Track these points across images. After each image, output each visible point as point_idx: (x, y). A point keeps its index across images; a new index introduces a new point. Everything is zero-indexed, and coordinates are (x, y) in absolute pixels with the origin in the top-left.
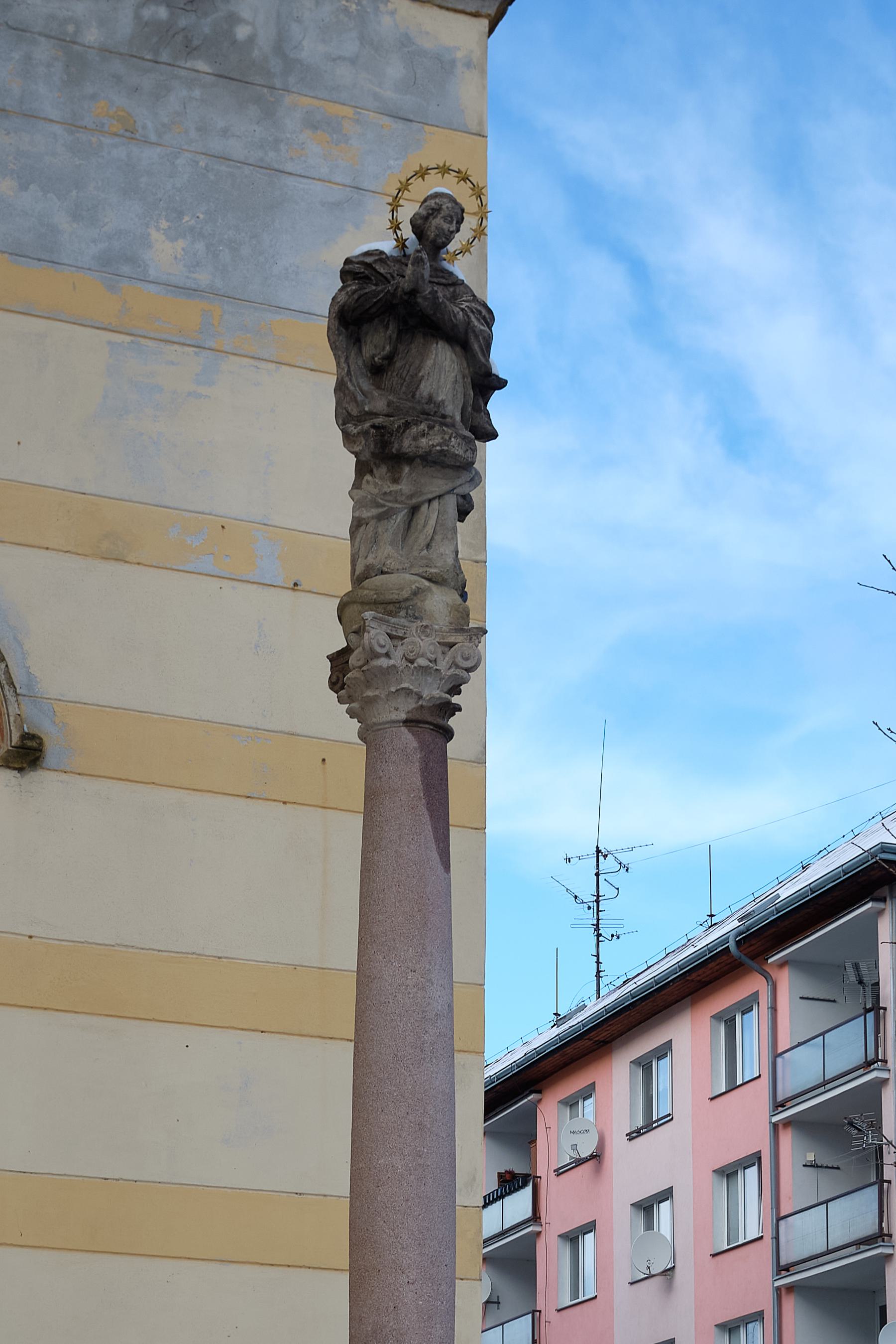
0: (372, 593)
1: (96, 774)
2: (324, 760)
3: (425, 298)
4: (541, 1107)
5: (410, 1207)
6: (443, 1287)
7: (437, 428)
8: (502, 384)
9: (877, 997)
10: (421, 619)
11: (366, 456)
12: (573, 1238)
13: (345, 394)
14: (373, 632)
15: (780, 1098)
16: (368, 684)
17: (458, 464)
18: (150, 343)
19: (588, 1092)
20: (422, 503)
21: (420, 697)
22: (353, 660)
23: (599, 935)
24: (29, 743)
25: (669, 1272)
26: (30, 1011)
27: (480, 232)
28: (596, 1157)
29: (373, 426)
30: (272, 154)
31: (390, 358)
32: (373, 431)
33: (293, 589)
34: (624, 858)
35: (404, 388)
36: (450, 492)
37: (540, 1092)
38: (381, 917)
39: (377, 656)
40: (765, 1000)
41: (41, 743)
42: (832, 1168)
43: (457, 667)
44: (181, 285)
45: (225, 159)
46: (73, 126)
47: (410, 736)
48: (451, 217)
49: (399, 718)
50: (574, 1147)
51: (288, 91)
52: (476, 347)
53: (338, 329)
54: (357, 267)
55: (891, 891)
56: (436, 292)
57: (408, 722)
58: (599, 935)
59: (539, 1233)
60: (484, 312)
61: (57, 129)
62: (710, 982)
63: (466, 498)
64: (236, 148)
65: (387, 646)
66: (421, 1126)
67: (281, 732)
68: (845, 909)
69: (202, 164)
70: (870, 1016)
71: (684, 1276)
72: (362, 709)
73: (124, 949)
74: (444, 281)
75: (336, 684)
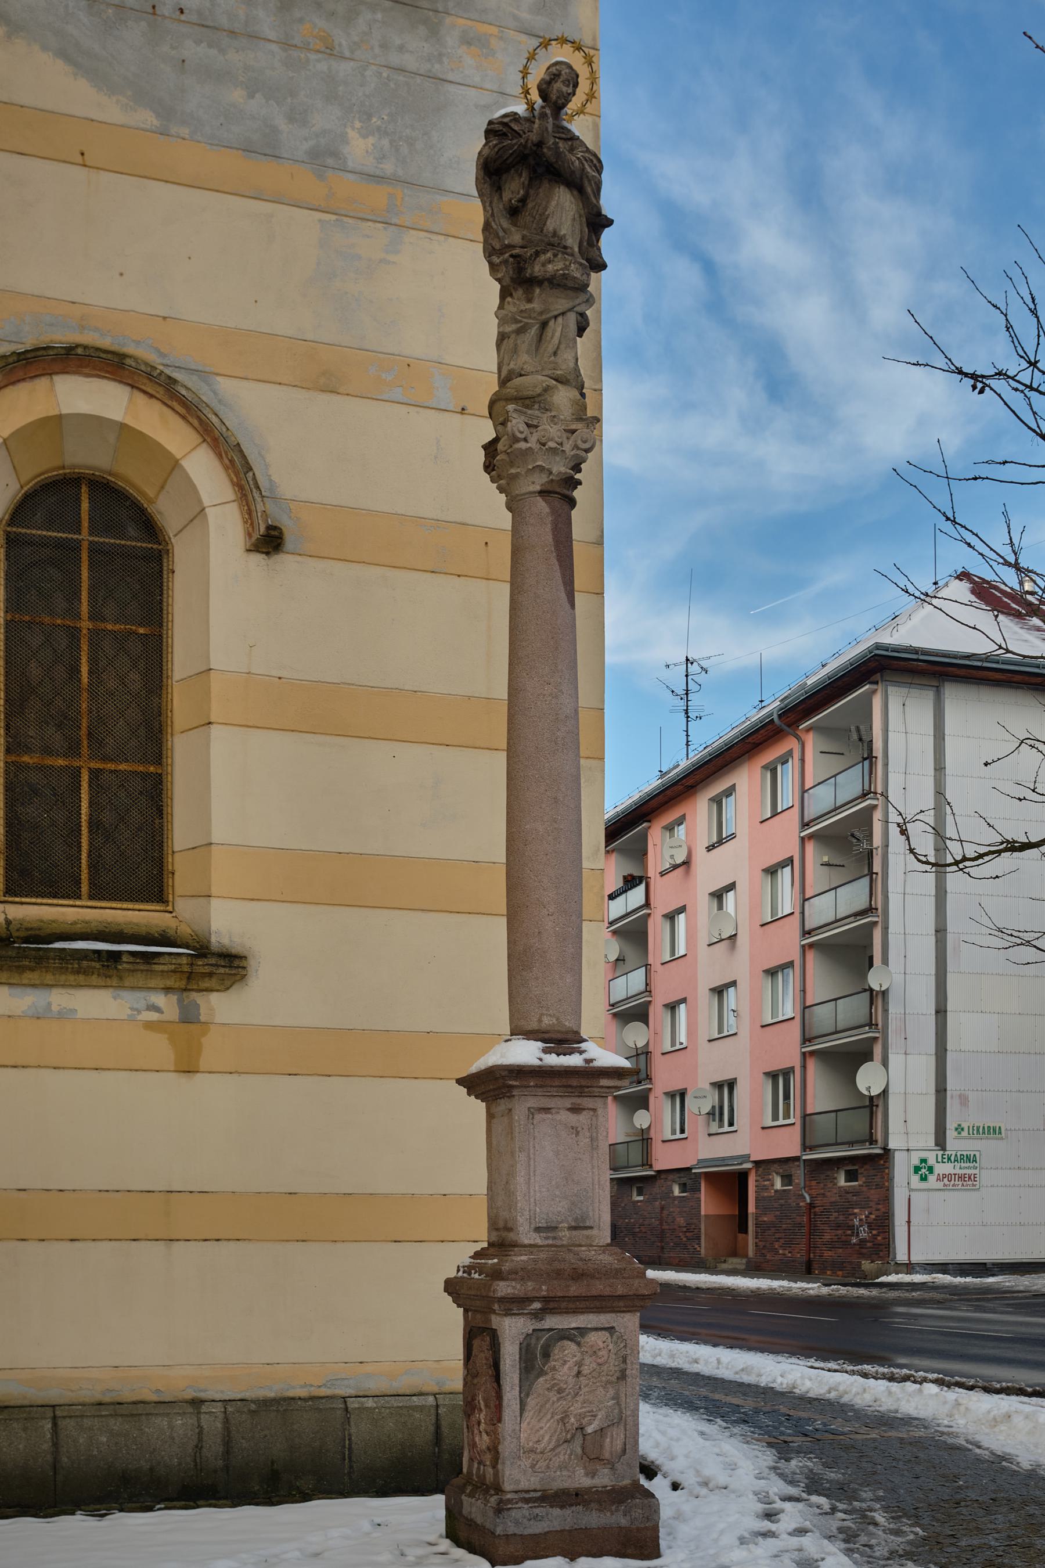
0: (513, 390)
1: (322, 555)
2: (486, 543)
3: (549, 148)
4: (650, 831)
5: (548, 860)
6: (574, 918)
7: (560, 256)
8: (609, 223)
9: (871, 750)
10: (550, 410)
11: (507, 281)
12: (671, 917)
13: (490, 233)
14: (514, 421)
15: (806, 820)
16: (512, 464)
17: (577, 286)
18: (350, 221)
19: (680, 821)
20: (549, 319)
21: (551, 473)
22: (500, 446)
23: (688, 717)
24: (273, 533)
25: (733, 937)
26: (282, 732)
27: (591, 96)
28: (687, 863)
29: (512, 256)
30: (437, 66)
31: (523, 200)
32: (511, 259)
33: (462, 413)
34: (704, 664)
35: (534, 225)
36: (570, 310)
37: (649, 821)
38: (524, 644)
39: (517, 440)
40: (797, 755)
41: (281, 533)
42: (840, 866)
43: (578, 448)
44: (372, 173)
45: (401, 70)
46: (286, 44)
47: (543, 504)
48: (569, 81)
49: (535, 490)
50: (672, 857)
51: (448, 14)
52: (589, 190)
53: (484, 178)
54: (497, 127)
55: (882, 676)
56: (558, 143)
57: (542, 493)
58: (688, 717)
59: (649, 915)
60: (595, 161)
61: (274, 47)
62: (761, 744)
63: (583, 315)
64: (410, 61)
65: (525, 433)
66: (556, 800)
67: (455, 522)
68: (850, 690)
69: (385, 75)
70: (867, 763)
71: (743, 940)
72: (508, 484)
73: (347, 686)
74: (563, 136)
75: (488, 467)
